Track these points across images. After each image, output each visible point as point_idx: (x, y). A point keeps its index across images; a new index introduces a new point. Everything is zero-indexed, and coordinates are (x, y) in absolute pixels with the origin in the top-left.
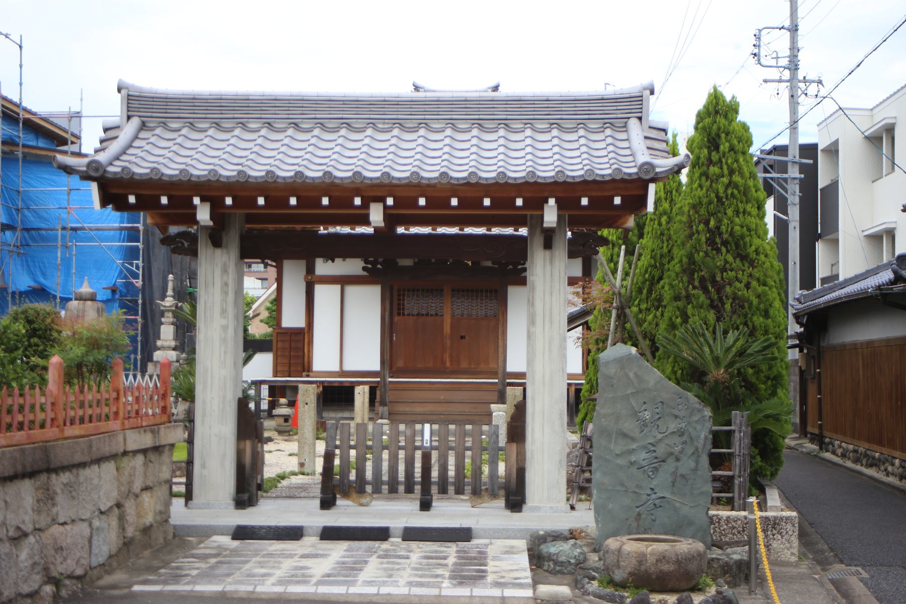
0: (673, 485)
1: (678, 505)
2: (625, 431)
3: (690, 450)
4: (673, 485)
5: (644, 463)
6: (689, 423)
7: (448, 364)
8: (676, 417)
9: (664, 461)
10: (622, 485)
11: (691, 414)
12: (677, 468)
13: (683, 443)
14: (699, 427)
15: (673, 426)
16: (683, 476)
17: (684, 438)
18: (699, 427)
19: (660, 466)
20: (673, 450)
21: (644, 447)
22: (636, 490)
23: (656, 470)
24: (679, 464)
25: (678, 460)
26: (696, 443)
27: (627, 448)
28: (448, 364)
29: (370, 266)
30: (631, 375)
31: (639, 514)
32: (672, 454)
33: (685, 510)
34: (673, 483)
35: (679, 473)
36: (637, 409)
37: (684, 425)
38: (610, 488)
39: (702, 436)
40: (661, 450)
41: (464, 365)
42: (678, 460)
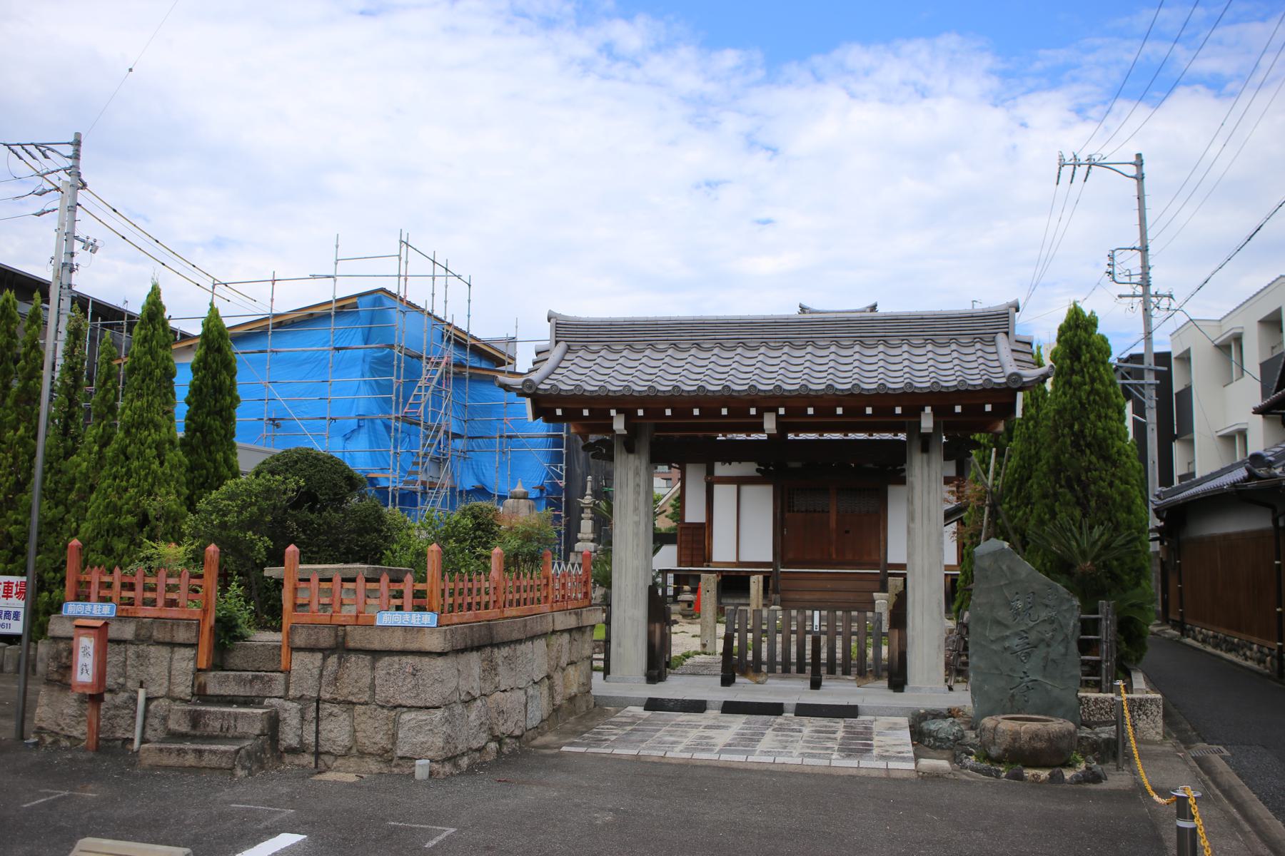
5: (1017, 649)
8: (1047, 606)
10: (997, 668)
12: (1048, 653)
15: (1044, 615)
16: (1053, 660)
21: (1017, 634)
25: (1048, 645)
30: (1004, 567)
31: (1013, 696)
32: (1043, 640)
34: (1045, 667)
40: (1033, 636)
42: (1048, 645)
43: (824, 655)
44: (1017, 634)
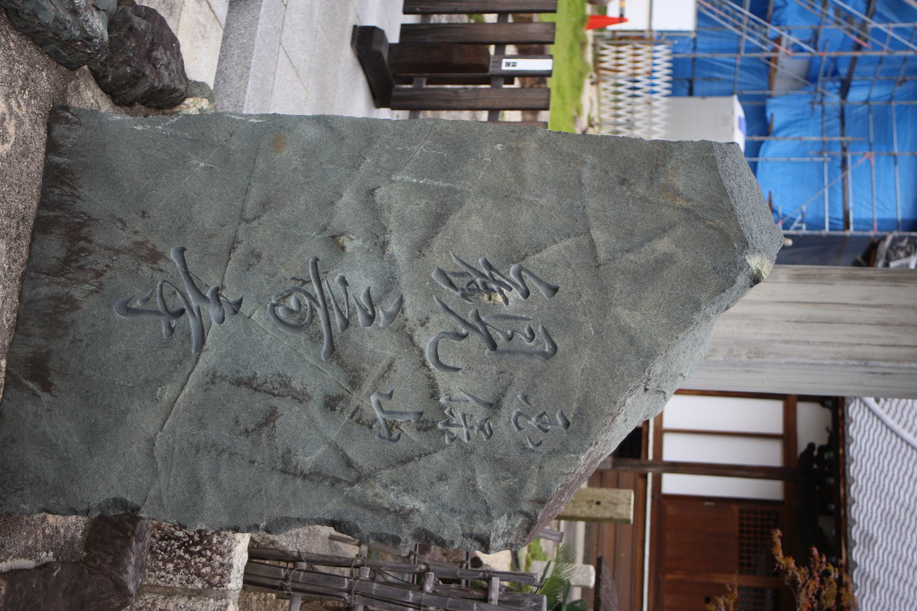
0: (239, 383)
1: (167, 392)
2: (454, 220)
3: (361, 452)
4: (239, 383)
5: (332, 282)
6: (467, 452)
7: (669, 577)
8: (494, 406)
9: (332, 348)
10: (265, 205)
11: (499, 463)
12: (301, 398)
13: (391, 426)
14: (447, 491)
15: (457, 389)
16: (271, 416)
17: (410, 433)
18: (447, 491)
19: (315, 338)
20: (367, 386)
21: (389, 283)
22: (241, 250)
23: (299, 323)
24: (315, 408)
25: (331, 404)
26: (386, 475)
27: (393, 225)
28: (669, 577)
29: (816, 453)
30: (663, 245)
31: (155, 256)
32: (355, 383)
33: (144, 421)
34: (250, 384)
35: (283, 405)
36: (531, 262)
37: (461, 432)
38: (261, 165)
39: (410, 502)
40: (375, 344)
41: (668, 601)
42: (331, 404)
43: (717, 75)
44: (389, 283)
